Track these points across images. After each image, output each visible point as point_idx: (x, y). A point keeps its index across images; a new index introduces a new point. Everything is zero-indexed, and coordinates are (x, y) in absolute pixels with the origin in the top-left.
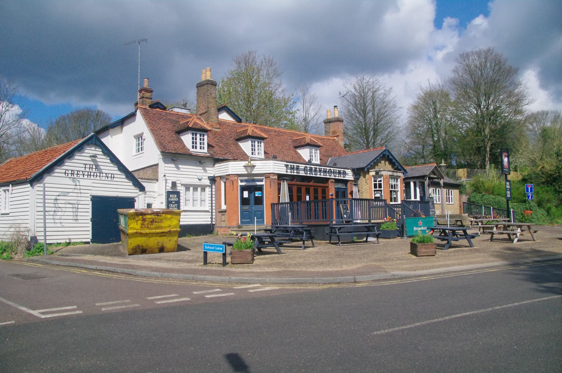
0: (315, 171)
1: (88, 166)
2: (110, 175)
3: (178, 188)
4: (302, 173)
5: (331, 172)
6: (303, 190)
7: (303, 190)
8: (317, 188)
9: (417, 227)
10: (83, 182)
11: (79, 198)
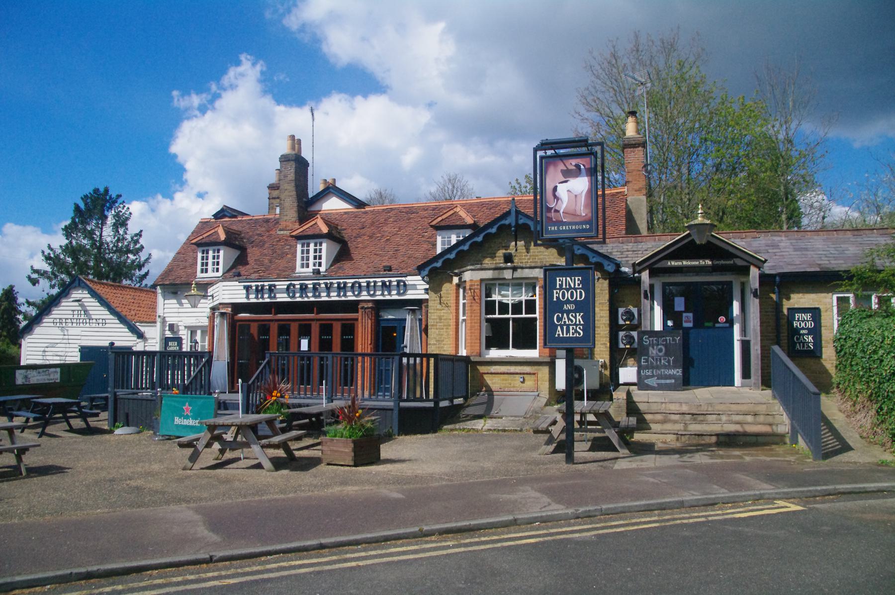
0: (315, 288)
1: (76, 312)
2: (64, 320)
3: (180, 333)
4: (282, 298)
5: (360, 286)
6: (294, 328)
7: (294, 328)
8: (352, 322)
9: (180, 417)
10: (72, 331)
11: (67, 350)
